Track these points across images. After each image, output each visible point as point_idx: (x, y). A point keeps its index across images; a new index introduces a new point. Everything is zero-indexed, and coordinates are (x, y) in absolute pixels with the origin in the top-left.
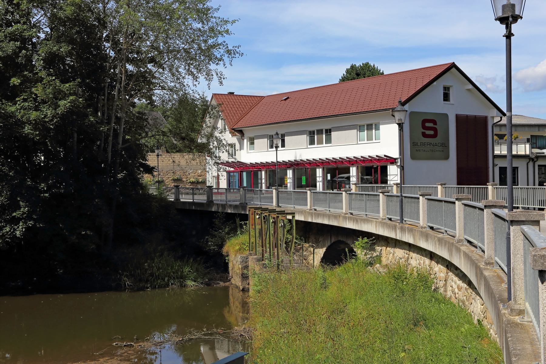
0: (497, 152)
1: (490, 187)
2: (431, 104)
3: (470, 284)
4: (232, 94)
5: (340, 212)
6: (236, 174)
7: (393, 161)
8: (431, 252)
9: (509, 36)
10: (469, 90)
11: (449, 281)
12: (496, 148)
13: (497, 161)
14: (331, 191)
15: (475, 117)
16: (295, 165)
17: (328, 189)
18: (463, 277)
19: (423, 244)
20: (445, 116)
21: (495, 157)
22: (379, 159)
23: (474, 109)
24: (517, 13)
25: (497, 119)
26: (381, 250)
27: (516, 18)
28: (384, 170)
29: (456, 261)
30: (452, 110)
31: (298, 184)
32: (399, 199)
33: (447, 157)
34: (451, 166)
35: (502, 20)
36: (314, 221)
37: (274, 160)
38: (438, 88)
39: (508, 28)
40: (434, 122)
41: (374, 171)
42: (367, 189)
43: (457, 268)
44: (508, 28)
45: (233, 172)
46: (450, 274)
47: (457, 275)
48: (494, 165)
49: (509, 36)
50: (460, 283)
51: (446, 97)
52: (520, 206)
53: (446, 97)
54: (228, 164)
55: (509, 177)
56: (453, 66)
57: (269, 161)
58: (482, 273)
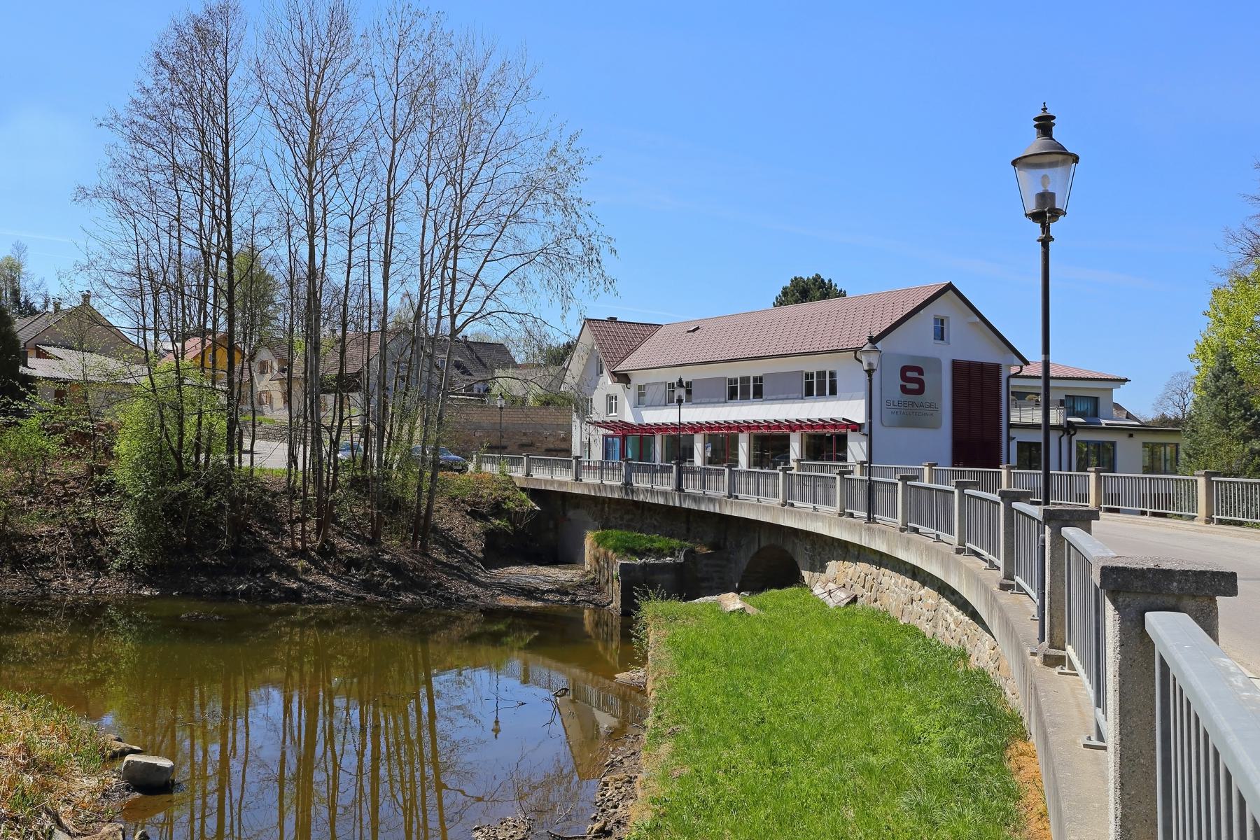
0: (1014, 419)
1: (1004, 472)
2: (916, 342)
3: (975, 616)
4: (613, 320)
5: (761, 503)
6: (617, 441)
7: (856, 427)
8: (915, 567)
9: (1045, 242)
10: (974, 323)
11: (942, 611)
12: (1012, 413)
13: (1013, 433)
14: (758, 470)
15: (982, 364)
16: (710, 429)
17: (756, 465)
18: (964, 605)
19: (902, 555)
20: (937, 362)
21: (1011, 426)
22: (835, 424)
23: (981, 352)
24: (1057, 206)
25: (1014, 370)
26: (999, 569)
27: (1056, 214)
28: (842, 442)
29: (953, 582)
30: (947, 354)
31: (759, 459)
32: (866, 485)
33: (1113, 444)
34: (941, 437)
35: (1036, 216)
36: (734, 514)
37: (676, 421)
38: (925, 322)
39: (1045, 229)
40: (920, 371)
41: (826, 443)
42: (810, 468)
43: (954, 592)
44: (1045, 229)
45: (612, 437)
46: (943, 600)
47: (953, 603)
48: (1009, 439)
49: (1045, 242)
50: (958, 614)
51: (940, 334)
52: (1148, 510)
53: (940, 334)
54: (605, 425)
55: (1031, 456)
56: (950, 287)
57: (668, 421)
58: (995, 600)
